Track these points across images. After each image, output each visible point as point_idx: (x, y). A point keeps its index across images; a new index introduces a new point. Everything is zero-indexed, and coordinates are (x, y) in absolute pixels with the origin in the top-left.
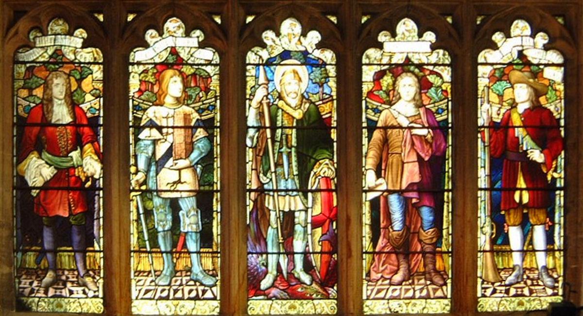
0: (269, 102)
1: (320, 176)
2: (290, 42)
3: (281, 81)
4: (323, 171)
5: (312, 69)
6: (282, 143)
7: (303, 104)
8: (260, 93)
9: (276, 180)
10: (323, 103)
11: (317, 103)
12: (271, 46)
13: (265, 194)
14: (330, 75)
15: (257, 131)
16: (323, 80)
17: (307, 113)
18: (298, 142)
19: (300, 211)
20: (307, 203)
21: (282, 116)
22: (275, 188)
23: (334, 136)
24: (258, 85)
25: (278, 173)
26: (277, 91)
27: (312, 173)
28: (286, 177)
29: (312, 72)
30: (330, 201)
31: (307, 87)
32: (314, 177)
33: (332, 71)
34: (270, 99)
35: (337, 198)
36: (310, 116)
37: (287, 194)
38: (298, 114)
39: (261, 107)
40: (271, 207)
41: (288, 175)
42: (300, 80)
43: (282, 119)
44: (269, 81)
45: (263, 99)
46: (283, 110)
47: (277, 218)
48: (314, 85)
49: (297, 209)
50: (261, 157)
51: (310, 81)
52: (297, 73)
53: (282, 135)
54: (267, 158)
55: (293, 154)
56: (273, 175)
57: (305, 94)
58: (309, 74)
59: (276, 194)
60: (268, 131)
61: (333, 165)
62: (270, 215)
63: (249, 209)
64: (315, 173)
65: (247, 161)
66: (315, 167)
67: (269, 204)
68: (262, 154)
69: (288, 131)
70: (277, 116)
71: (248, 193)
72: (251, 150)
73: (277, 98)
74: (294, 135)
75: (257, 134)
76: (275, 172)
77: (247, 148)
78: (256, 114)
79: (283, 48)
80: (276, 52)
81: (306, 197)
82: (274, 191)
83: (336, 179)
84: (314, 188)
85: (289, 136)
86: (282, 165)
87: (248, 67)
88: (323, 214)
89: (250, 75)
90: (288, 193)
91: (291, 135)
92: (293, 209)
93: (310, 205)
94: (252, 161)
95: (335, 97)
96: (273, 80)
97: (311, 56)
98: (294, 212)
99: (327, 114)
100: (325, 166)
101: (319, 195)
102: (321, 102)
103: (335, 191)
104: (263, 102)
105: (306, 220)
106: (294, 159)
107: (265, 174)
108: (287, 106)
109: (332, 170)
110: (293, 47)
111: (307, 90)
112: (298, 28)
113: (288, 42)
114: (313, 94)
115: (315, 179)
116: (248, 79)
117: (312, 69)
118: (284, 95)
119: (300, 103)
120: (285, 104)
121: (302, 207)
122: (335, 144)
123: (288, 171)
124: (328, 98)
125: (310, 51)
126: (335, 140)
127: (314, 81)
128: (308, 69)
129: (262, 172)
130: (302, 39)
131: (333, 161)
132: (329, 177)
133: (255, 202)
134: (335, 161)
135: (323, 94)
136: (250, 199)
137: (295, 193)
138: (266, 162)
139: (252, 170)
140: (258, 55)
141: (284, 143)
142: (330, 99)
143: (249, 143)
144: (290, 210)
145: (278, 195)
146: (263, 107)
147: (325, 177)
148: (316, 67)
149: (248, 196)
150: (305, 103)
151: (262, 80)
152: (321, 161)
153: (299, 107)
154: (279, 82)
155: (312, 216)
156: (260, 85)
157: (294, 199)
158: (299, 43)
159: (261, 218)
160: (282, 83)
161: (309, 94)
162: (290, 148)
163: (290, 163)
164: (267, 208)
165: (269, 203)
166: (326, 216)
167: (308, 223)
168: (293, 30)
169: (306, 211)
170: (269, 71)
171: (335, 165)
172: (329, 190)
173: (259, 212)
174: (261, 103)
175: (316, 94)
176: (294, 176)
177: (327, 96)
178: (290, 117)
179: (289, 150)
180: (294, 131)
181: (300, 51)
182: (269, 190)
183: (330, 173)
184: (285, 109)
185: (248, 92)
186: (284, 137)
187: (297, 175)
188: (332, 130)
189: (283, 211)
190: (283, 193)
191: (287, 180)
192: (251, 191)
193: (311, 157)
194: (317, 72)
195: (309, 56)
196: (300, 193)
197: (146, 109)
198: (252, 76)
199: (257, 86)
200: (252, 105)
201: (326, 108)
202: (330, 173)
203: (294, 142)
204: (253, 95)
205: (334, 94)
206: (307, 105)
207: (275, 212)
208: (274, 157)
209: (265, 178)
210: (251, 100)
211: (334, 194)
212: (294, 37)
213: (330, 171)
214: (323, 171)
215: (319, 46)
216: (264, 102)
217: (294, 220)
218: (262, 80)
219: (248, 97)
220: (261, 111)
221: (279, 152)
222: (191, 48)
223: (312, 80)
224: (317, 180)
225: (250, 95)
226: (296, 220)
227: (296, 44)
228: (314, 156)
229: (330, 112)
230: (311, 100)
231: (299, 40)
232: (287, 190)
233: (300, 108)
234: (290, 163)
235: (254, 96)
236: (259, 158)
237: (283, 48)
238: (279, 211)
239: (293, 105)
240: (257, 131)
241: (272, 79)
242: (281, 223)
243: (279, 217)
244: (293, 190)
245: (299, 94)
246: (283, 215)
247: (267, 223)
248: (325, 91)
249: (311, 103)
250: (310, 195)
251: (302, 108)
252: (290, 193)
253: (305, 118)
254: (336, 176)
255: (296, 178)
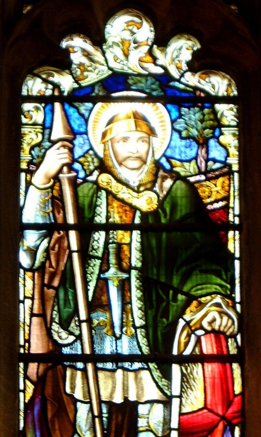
0: (77, 177)
1: (202, 328)
2: (126, 56)
3: (104, 135)
4: (209, 318)
5: (179, 111)
6: (108, 260)
7: (159, 180)
8: (55, 159)
9: (91, 337)
10: (208, 179)
11: (192, 179)
12: (81, 65)
13: (65, 368)
14: (225, 121)
15: (44, 237)
16: (207, 131)
17: (167, 200)
18: (144, 259)
19: (152, 402)
20: (169, 387)
21: (108, 205)
22: (88, 351)
23: (234, 244)
24: (49, 140)
25: (96, 322)
26: (96, 155)
27: (181, 323)
28: (117, 331)
29: (180, 116)
30: (226, 380)
31: (168, 147)
32: (185, 333)
33: (228, 113)
34: (77, 171)
35: (243, 376)
36: (174, 206)
37: (118, 368)
38: (146, 202)
39: (57, 188)
40: (79, 394)
41: (122, 327)
42: (152, 132)
43: (108, 212)
44: (73, 133)
45: (60, 171)
46: (109, 193)
47: (94, 417)
48: (184, 142)
49: (143, 400)
50: (56, 289)
51: (176, 135)
52: (144, 119)
53: (107, 243)
54: (71, 291)
55: (135, 283)
56: (84, 326)
57: (164, 161)
58: (173, 122)
59: (90, 367)
60: (73, 235)
61: (234, 308)
62: (76, 411)
63: (23, 399)
64: (188, 323)
65: (21, 298)
66: (188, 311)
67: (73, 388)
68: (57, 281)
69: (122, 236)
70: (96, 206)
71: (21, 365)
72: (29, 274)
73: (96, 168)
74: (136, 244)
75: (46, 241)
76: (89, 321)
77: (22, 271)
78: (45, 203)
79: (110, 69)
80: (92, 78)
81: (167, 375)
82: (84, 358)
83: (239, 337)
84: (187, 352)
85: (125, 248)
86: (108, 307)
87: (27, 107)
88: (210, 411)
89: (31, 122)
90: (120, 364)
91: (129, 245)
92: (132, 397)
93: (176, 390)
94: (32, 299)
95: (235, 168)
96: (86, 133)
97: (177, 84)
98: (136, 404)
99: (217, 201)
100: (214, 308)
101: (197, 370)
102: (203, 177)
103: (239, 358)
104: (61, 175)
105: (167, 422)
106: (135, 294)
107: (65, 325)
108: (120, 186)
109: (230, 317)
110: (133, 64)
111: (169, 153)
112: (146, 32)
113: (122, 57)
114: (181, 161)
115: (189, 336)
116: (25, 130)
117: (179, 111)
118: (112, 162)
119: (150, 178)
120: (114, 182)
121: (156, 395)
122: (237, 263)
123: (122, 319)
124: (221, 168)
125: (175, 74)
126: (237, 255)
127: (184, 134)
128: (169, 112)
129: (57, 320)
130: (157, 51)
131: (233, 299)
132: (224, 333)
133: (39, 384)
134: (238, 297)
135: (207, 160)
136: (26, 377)
137: (137, 365)
138: (66, 300)
139: (32, 315)
140: (52, 83)
141: (112, 260)
142: (226, 170)
143: (24, 260)
144: (126, 399)
145: (96, 370)
146: (61, 186)
147: (213, 331)
148: (189, 108)
149: (21, 370)
150: (164, 178)
151: (59, 131)
152: (203, 299)
153: (149, 186)
154: (100, 136)
155: (181, 414)
156: (54, 143)
157: (136, 377)
158: (149, 58)
159: (53, 416)
160: (108, 138)
161: (173, 161)
162: (128, 271)
163: (125, 302)
164: (71, 396)
165: (75, 385)
166: (217, 414)
167: (171, 429)
168: (133, 33)
169: (167, 402)
170: (76, 115)
171: (238, 307)
172: (222, 358)
173: (49, 407)
174: (56, 178)
175: (189, 161)
176: (135, 328)
177: (218, 165)
178: (127, 208)
179: (125, 276)
180: (136, 234)
181: (151, 75)
182: (74, 358)
183: (227, 323)
184: (114, 190)
185: (25, 156)
186: (112, 248)
187: (141, 327)
188: (231, 234)
189: (110, 404)
190: (109, 365)
191: (118, 338)
192: (29, 358)
193: (178, 291)
194: (193, 115)
195: (172, 84)
196: (152, 365)
197: (173, 64)
198: (35, 124)
199: (47, 144)
200: (33, 181)
201: (214, 189)
202: (222, 323)
203: (136, 259)
204: (35, 164)
205: (234, 161)
206: (168, 183)
207: (88, 406)
208: (86, 291)
209: (64, 334)
210: (30, 172)
211: (235, 366)
212: (136, 48)
213: (225, 318)
214: (209, 318)
215: (195, 66)
216: (65, 176)
217: (136, 422)
218: (59, 131)
219: (24, 166)
220: (56, 193)
221: (99, 278)
222: (119, 63)
223: (179, 132)
224: (193, 338)
225: (30, 163)
226: (142, 423)
227: (140, 60)
228: (185, 289)
229: (226, 198)
230: (178, 173)
231: (150, 52)
232: (117, 358)
233: (151, 189)
234: (125, 302)
235: (38, 166)
236: (51, 292)
237: (110, 69)
238: (100, 402)
239: (134, 183)
240: (44, 237)
241: (82, 130)
242: (103, 429)
243: (100, 416)
244: (132, 358)
245: (150, 160)
246: (109, 412)
247: (70, 427)
248: (211, 155)
249: (177, 177)
250: (176, 369)
251: (157, 188)
252: (127, 365)
253: (164, 211)
254: (240, 330)
255: (140, 333)
